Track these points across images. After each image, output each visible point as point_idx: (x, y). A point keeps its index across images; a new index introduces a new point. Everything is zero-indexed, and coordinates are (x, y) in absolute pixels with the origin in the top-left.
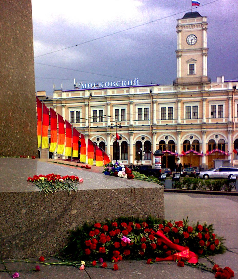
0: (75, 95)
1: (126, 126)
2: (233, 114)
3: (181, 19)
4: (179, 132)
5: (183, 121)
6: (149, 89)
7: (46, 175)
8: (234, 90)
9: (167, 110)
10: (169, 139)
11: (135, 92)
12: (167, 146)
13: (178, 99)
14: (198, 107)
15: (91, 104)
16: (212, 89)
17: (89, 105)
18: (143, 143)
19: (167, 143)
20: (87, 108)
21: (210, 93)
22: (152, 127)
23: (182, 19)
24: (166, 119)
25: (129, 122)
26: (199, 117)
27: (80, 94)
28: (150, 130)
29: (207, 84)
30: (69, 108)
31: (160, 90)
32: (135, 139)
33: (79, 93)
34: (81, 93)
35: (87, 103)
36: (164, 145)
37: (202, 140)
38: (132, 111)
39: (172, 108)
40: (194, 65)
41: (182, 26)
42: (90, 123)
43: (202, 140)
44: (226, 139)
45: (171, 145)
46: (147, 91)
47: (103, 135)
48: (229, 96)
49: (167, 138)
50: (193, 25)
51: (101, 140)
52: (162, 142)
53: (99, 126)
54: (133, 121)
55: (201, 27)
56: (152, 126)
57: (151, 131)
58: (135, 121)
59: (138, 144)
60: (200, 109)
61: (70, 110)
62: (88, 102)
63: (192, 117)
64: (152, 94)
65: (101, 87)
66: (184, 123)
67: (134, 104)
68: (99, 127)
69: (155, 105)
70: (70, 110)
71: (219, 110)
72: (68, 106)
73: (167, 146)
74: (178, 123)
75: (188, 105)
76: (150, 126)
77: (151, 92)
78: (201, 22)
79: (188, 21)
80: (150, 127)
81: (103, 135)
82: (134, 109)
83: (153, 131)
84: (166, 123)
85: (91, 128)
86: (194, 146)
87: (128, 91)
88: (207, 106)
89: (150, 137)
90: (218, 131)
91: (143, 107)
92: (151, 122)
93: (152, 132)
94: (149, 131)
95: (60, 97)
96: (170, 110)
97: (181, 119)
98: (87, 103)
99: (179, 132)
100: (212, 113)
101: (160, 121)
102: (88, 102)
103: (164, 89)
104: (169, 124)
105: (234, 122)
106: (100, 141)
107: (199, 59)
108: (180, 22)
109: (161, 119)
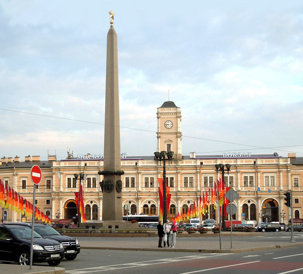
0: (207, 162)
1: (97, 192)
2: (201, 183)
3: (160, 107)
4: (282, 198)
5: (263, 188)
6: (134, 162)
7: (275, 232)
8: (201, 166)
9: (249, 178)
10: (151, 203)
11: (241, 163)
12: (150, 209)
13: (158, 171)
14: (275, 177)
15: (202, 171)
16: (184, 164)
17: (201, 172)
18: (91, 207)
19: (149, 207)
20: (199, 175)
21: (183, 168)
22: (257, 193)
23: (161, 107)
24: (248, 186)
25: (99, 189)
26: (254, 185)
27: (77, 164)
28: (255, 195)
29: (180, 160)
30: (242, 173)
31: (242, 162)
32: (142, 203)
33: (231, 160)
34: (77, 162)
35: (83, 172)
36: (174, 208)
37: (177, 205)
38: (179, 179)
39: (247, 177)
40: (170, 144)
41: (161, 113)
42: (85, 188)
43: (177, 205)
44: (98, 204)
45: (153, 208)
46: (252, 162)
47: (277, 198)
48: (198, 171)
49: (249, 202)
50: (164, 113)
51: (172, 203)
52: (146, 206)
53: (92, 191)
54: (240, 187)
55: (175, 115)
56: (137, 193)
57: (136, 197)
58: (143, 188)
59: (245, 206)
60: (283, 180)
61: (184, 176)
62: (200, 170)
63: (249, 186)
64: (137, 167)
65: (235, 157)
66: (124, 190)
67: (65, 174)
68: (150, 192)
69: (140, 175)
70: (184, 176)
71: (230, 181)
72: (242, 171)
73: (150, 209)
74: (238, 190)
75: (186, 176)
76: (136, 192)
77: (136, 164)
78: (175, 111)
79: (166, 110)
80: (201, 193)
81: (277, 198)
82: (181, 178)
83: (138, 197)
84: (70, 191)
85: (85, 192)
86: (151, 209)
87: (236, 162)
88: (142, 178)
89: (255, 201)
90: (249, 197)
91: (149, 177)
92: (256, 188)
93: (257, 197)
94: (134, 197)
95: (278, 162)
96: (152, 180)
97: (283, 186)
98: (199, 171)
99: (282, 198)
100: (245, 183)
101: (144, 189)
102: (84, 171)
103: (246, 162)
104: (151, 191)
105: (202, 191)
106: (93, 204)
107: (174, 140)
108: (160, 110)
109: (145, 187)
